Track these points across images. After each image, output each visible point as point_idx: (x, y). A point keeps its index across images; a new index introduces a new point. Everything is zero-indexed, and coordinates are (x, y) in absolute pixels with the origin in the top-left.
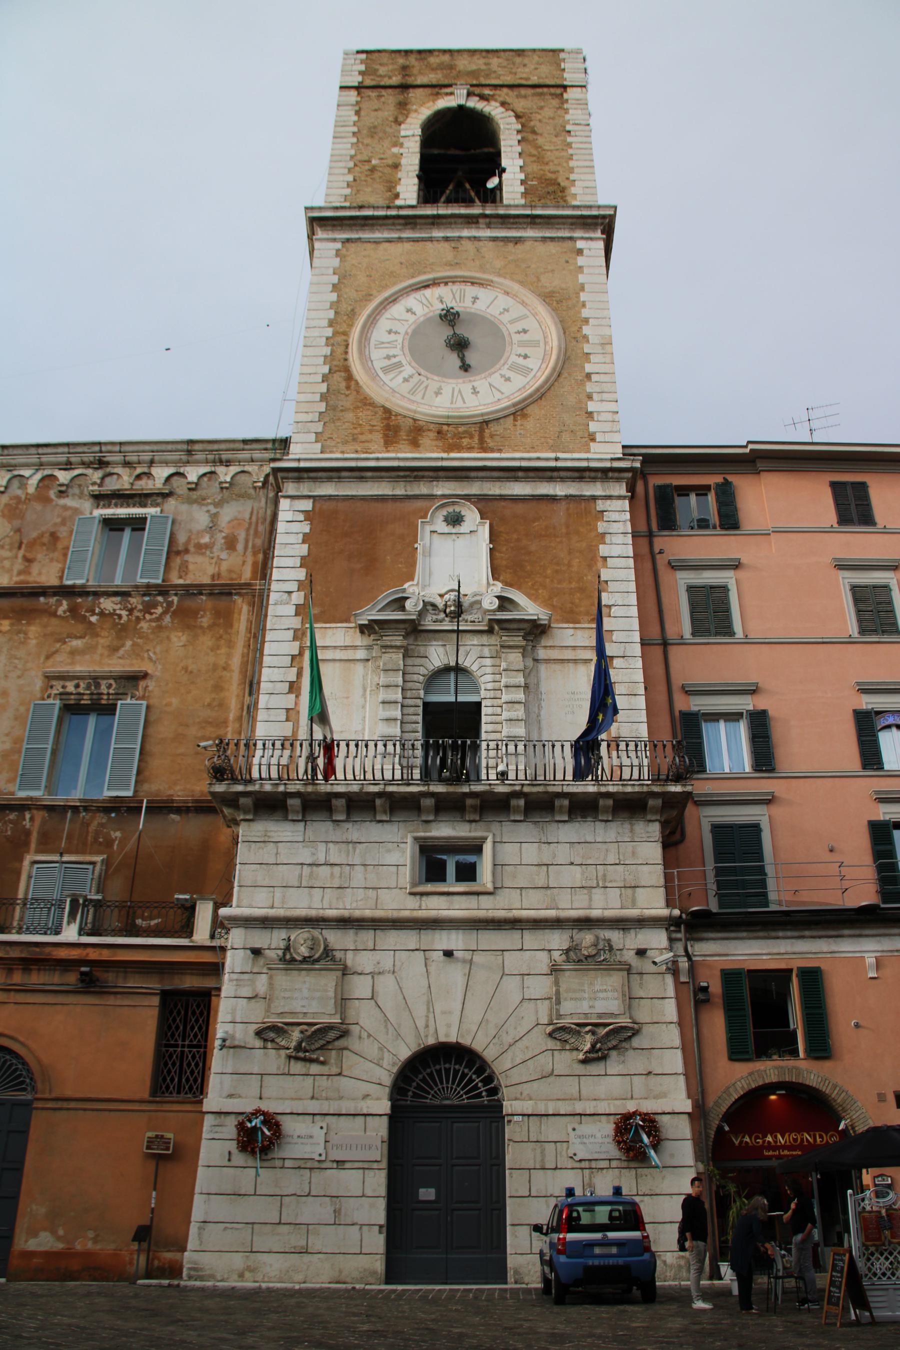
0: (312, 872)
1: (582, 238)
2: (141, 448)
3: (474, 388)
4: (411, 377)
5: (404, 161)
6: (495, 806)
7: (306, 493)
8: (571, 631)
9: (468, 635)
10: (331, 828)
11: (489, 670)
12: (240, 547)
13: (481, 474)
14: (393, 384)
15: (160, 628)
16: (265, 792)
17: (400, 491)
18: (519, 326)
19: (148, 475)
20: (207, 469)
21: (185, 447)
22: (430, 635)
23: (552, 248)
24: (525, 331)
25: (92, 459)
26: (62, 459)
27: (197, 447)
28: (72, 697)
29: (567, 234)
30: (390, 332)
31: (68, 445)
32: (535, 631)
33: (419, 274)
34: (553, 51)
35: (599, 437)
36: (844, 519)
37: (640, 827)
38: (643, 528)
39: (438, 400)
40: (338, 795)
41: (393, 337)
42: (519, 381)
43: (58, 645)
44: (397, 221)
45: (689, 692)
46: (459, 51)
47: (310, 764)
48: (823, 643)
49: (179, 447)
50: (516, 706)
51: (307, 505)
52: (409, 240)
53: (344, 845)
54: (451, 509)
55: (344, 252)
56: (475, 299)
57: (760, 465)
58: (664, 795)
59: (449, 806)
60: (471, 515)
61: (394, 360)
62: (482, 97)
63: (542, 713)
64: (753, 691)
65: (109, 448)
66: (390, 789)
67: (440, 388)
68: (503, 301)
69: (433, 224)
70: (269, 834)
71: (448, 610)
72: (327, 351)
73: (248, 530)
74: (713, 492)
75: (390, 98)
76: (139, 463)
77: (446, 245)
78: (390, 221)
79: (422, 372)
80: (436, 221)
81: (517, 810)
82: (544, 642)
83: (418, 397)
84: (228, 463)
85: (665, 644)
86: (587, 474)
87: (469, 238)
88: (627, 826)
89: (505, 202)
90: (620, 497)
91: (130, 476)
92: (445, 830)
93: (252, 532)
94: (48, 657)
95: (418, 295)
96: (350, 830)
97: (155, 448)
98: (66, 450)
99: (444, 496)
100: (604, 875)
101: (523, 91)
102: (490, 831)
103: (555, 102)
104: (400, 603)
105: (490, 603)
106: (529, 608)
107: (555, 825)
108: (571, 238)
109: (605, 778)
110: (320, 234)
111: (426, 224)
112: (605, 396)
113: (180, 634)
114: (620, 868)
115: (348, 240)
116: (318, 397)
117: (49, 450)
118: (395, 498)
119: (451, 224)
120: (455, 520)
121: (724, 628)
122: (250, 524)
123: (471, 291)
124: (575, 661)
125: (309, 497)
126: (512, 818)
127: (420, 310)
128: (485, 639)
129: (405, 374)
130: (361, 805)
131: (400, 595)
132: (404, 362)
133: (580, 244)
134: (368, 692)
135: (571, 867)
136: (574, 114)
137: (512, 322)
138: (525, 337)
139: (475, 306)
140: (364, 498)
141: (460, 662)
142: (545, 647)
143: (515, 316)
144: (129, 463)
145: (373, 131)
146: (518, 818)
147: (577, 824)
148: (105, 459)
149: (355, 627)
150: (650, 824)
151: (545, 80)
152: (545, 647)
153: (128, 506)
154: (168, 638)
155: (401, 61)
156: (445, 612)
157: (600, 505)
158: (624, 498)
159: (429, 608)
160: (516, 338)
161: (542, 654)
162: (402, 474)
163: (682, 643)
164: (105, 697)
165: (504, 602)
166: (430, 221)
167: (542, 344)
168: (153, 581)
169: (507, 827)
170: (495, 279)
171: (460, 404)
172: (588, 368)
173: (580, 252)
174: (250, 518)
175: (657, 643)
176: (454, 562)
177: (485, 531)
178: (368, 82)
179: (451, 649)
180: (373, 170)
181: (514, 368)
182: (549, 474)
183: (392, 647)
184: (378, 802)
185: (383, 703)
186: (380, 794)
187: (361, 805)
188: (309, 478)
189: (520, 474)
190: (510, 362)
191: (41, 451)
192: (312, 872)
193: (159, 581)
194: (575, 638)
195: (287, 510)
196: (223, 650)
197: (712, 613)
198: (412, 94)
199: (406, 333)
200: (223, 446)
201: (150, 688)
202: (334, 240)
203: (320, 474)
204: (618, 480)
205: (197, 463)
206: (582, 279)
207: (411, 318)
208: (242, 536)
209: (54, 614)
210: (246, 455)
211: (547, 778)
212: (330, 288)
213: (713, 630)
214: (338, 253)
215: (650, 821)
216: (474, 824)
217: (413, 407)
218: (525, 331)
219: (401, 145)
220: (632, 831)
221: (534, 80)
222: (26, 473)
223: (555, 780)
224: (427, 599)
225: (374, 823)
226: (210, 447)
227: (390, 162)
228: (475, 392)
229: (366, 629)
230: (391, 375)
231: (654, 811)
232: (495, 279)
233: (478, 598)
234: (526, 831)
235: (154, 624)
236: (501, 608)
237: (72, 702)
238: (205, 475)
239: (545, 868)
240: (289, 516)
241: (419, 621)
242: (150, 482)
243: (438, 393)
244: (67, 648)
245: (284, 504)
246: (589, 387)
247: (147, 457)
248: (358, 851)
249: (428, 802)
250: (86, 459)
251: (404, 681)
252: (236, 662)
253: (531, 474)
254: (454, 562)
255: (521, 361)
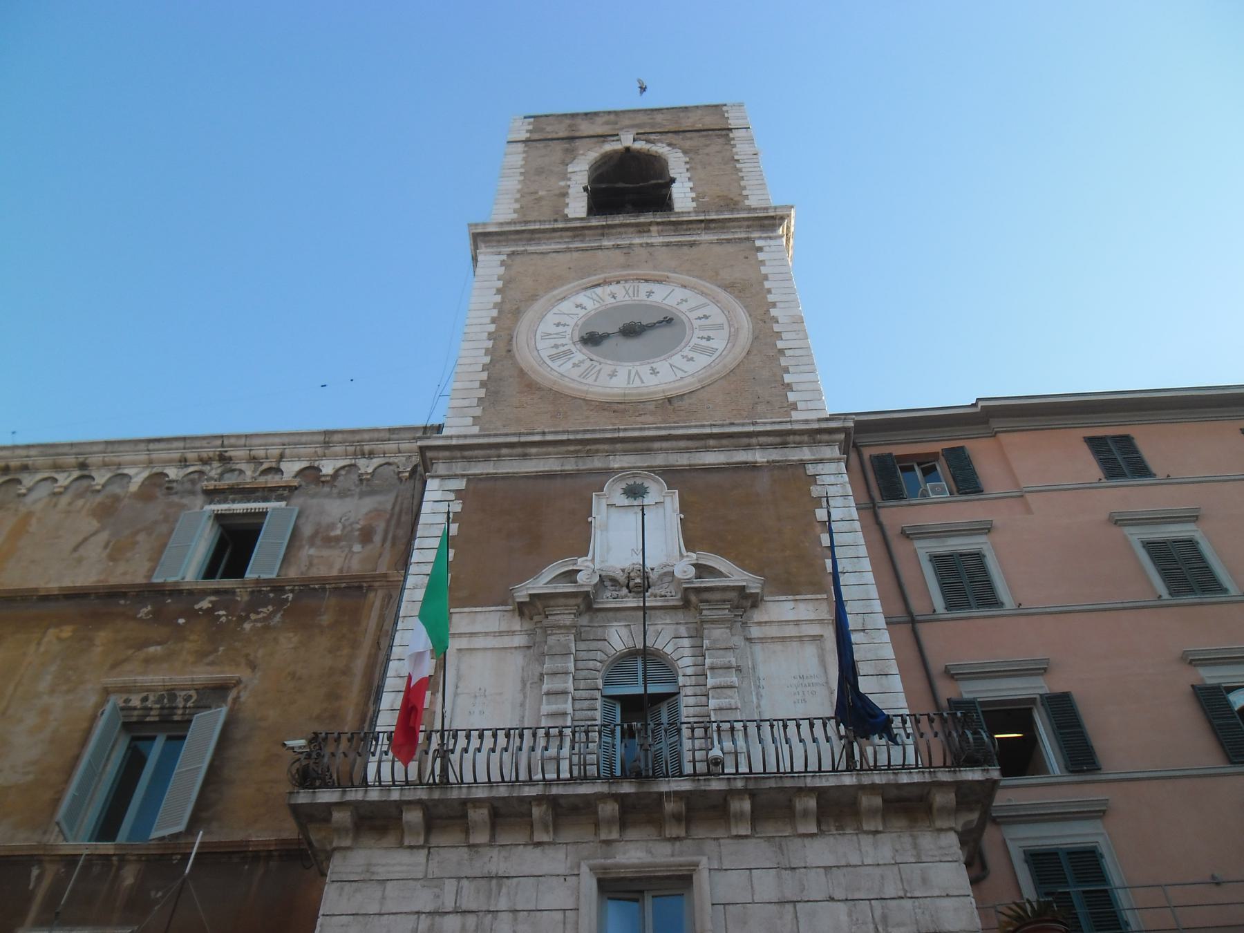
0: (433, 924)
1: (760, 238)
2: (271, 440)
3: (652, 369)
4: (582, 362)
5: (570, 191)
6: (705, 811)
7: (459, 472)
8: (791, 604)
9: (658, 613)
10: (466, 856)
11: (687, 652)
12: (377, 538)
13: (665, 445)
14: (561, 370)
15: (267, 628)
16: (369, 802)
17: (570, 466)
18: (700, 313)
19: (278, 470)
20: (347, 462)
21: (321, 438)
22: (611, 614)
23: (730, 248)
24: (706, 317)
25: (211, 454)
26: (176, 455)
27: (336, 438)
28: (136, 713)
29: (743, 235)
30: (558, 325)
31: (184, 439)
32: (745, 601)
33: (589, 275)
34: (716, 106)
35: (800, 406)
36: (1112, 470)
37: (927, 840)
38: (864, 500)
39: (614, 382)
40: (477, 803)
41: (561, 329)
42: (703, 360)
43: (130, 652)
44: (565, 234)
45: (951, 675)
46: (624, 112)
47: (438, 760)
48: (1124, 609)
49: (316, 438)
50: (728, 692)
51: (461, 484)
52: (577, 249)
53: (483, 882)
54: (631, 482)
55: (509, 262)
56: (650, 293)
57: (996, 424)
58: (959, 786)
59: (638, 813)
60: (656, 491)
61: (562, 349)
62: (648, 141)
63: (763, 703)
64: (1040, 670)
65: (233, 441)
66: (555, 791)
67: (615, 371)
68: (680, 293)
69: (603, 235)
70: (375, 869)
71: (631, 584)
72: (490, 344)
73: (388, 522)
74: (942, 459)
75: (559, 147)
76: (267, 458)
77: (617, 251)
78: (558, 234)
79: (594, 357)
80: (604, 230)
81: (740, 816)
82: (758, 616)
83: (590, 380)
84: (371, 455)
85: (912, 621)
86: (791, 438)
87: (641, 245)
88: (907, 839)
89: (676, 210)
90: (831, 460)
91: (254, 471)
92: (637, 853)
93: (393, 522)
94: (114, 666)
95: (589, 293)
96: (495, 859)
97: (286, 440)
98: (181, 444)
99: (622, 469)
100: (885, 918)
101: (688, 135)
102: (704, 854)
103: (721, 141)
104: (571, 575)
105: (684, 569)
106: (735, 575)
107: (798, 841)
108: (748, 239)
109: (865, 767)
110: (483, 249)
111: (594, 235)
112: (802, 368)
113: (291, 635)
114: (907, 904)
115: (513, 253)
116: (477, 384)
117: (162, 445)
118: (565, 475)
119: (620, 233)
120: (635, 492)
121: (989, 598)
122: (392, 515)
123: (645, 287)
124: (801, 639)
125: (463, 476)
126: (734, 832)
127: (590, 305)
128: (680, 616)
129: (575, 360)
130: (507, 815)
131: (571, 568)
132: (574, 349)
133: (758, 243)
134: (528, 685)
135: (830, 904)
136: (741, 150)
137: (691, 310)
138: (708, 322)
139: (651, 299)
140: (527, 477)
141: (648, 644)
142: (759, 623)
143: (694, 305)
144: (254, 458)
145: (540, 171)
146: (744, 833)
147: (832, 839)
148: (227, 454)
149: (513, 610)
150: (942, 835)
151: (711, 130)
152: (759, 623)
153: (249, 501)
154: (276, 640)
155: (568, 122)
156: (628, 587)
157: (811, 469)
158: (839, 460)
159: (607, 583)
160: (696, 323)
161: (755, 632)
162: (572, 448)
163: (933, 617)
164: (180, 712)
165: (702, 570)
166: (600, 231)
167: (726, 326)
168: (264, 576)
169: (728, 846)
170: (670, 274)
171: (637, 383)
172: (780, 345)
173: (760, 249)
174: (393, 508)
175: (907, 622)
176: (635, 534)
177: (672, 502)
178: (536, 136)
179: (637, 628)
180: (539, 200)
181: (697, 348)
182: (745, 441)
183: (560, 627)
184: (536, 812)
185: (548, 694)
186: (539, 799)
187: (507, 815)
188: (463, 457)
189: (712, 442)
190: (691, 344)
191: (151, 446)
192: (433, 924)
193: (274, 576)
194: (799, 612)
195: (435, 491)
196: (346, 651)
197: (967, 582)
198: (578, 143)
199: (576, 325)
200: (366, 436)
201: (242, 699)
202: (499, 253)
203: (476, 453)
204: (829, 443)
205: (335, 456)
206: (764, 270)
207: (582, 312)
208: (381, 526)
209: (134, 618)
210: (392, 446)
211: (782, 770)
212: (494, 291)
213: (973, 603)
214: (503, 263)
215: (940, 830)
216: (678, 844)
217: (585, 388)
218: (706, 317)
219: (569, 179)
220: (915, 846)
221: (699, 126)
222: (130, 471)
223: (792, 771)
224: (603, 574)
225: (530, 848)
226: (350, 437)
227: (557, 192)
228: (654, 372)
229: (523, 610)
230: (560, 362)
231: (945, 811)
232: (670, 274)
233: (670, 569)
234: (756, 852)
235: (259, 625)
236: (698, 577)
237: (134, 719)
238: (343, 468)
239: (789, 907)
240: (438, 495)
241: (596, 595)
242: (277, 478)
243: (613, 375)
244: (142, 655)
245: (432, 484)
246: (783, 362)
247: (275, 452)
248: (504, 890)
249: (609, 809)
250: (205, 455)
251: (576, 670)
252: (360, 664)
253: (725, 442)
254: (635, 534)
255: (704, 342)
